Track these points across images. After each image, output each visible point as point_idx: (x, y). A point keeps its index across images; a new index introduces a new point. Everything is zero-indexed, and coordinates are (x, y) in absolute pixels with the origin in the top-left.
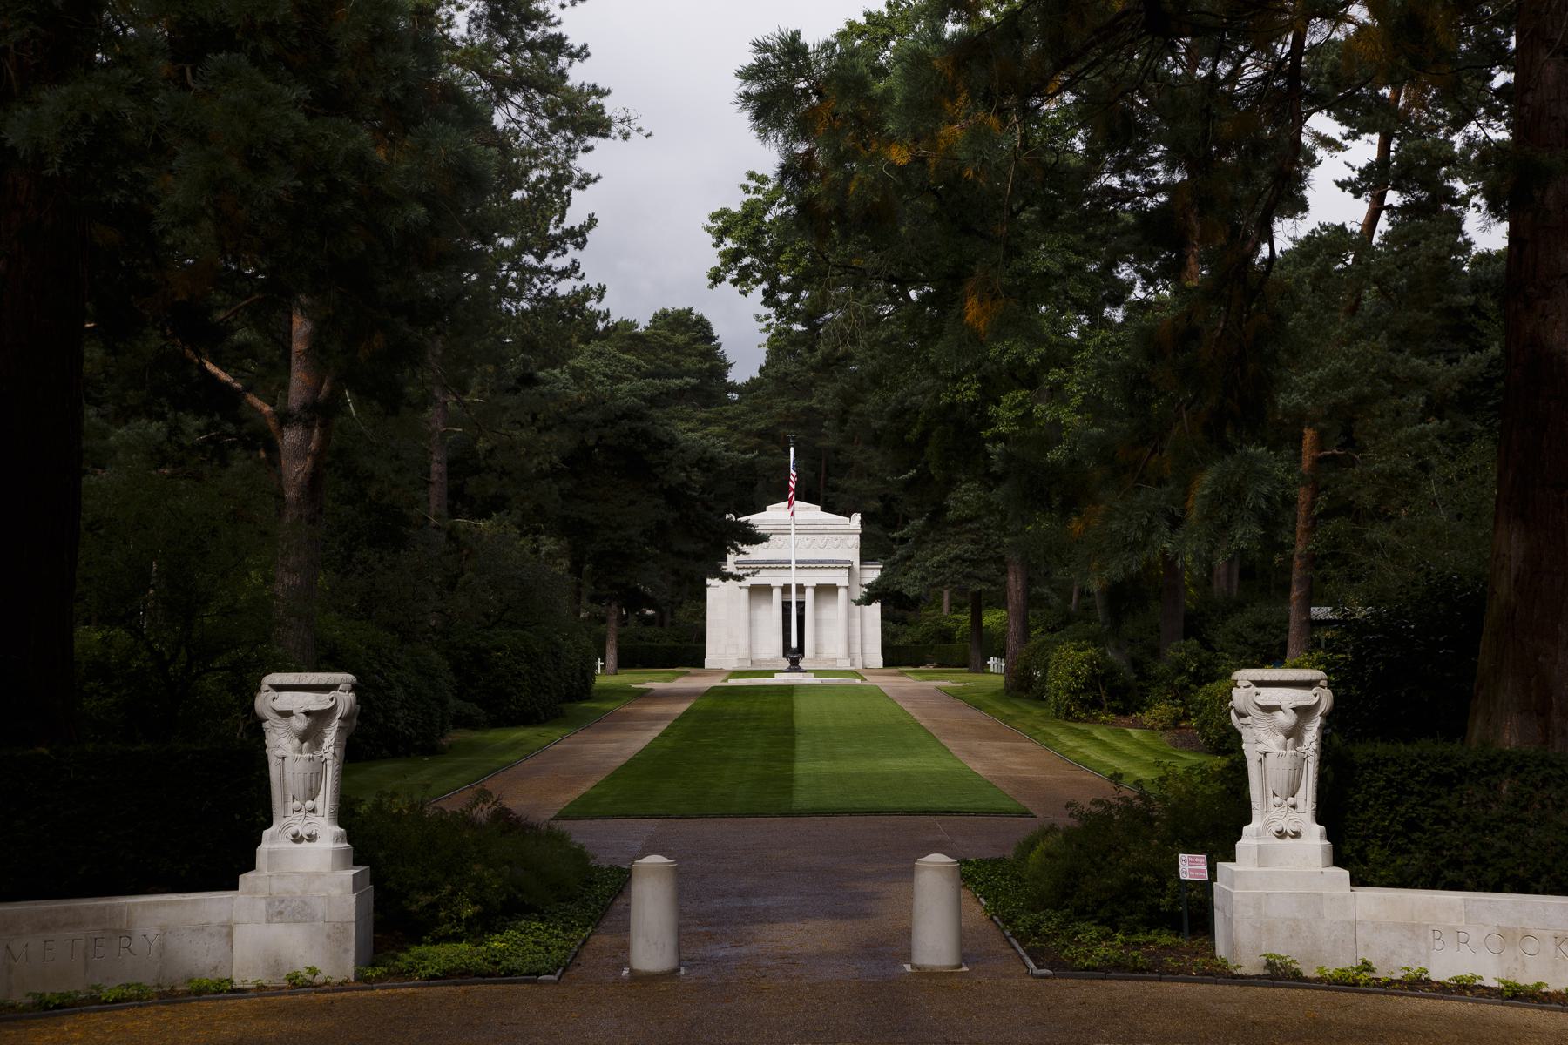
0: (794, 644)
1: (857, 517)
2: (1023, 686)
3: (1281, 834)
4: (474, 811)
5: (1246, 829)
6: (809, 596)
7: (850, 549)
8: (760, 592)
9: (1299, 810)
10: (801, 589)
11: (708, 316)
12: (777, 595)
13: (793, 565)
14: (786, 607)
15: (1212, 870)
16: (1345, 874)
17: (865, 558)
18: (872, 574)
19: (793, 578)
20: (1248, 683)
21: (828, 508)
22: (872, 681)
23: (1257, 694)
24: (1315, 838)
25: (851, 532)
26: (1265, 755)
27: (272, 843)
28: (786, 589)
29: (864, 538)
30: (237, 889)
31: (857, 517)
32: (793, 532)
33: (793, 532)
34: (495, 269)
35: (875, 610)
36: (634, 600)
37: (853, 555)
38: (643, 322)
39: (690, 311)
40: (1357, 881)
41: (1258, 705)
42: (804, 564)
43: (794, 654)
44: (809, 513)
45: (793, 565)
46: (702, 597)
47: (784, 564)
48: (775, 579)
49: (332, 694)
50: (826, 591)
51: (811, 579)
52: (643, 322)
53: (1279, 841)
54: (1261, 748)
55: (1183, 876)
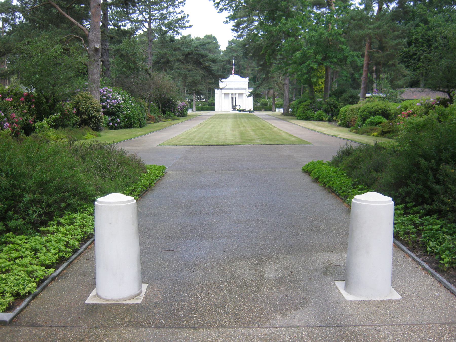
0: (234, 105)
1: (248, 78)
2: (286, 113)
6: (237, 96)
10: (235, 94)
11: (216, 37)
12: (230, 96)
13: (234, 89)
14: (232, 98)
17: (249, 87)
18: (251, 90)
19: (234, 92)
21: (241, 76)
28: (232, 94)
31: (248, 78)
34: (87, 14)
35: (251, 98)
36: (199, 93)
38: (226, 49)
39: (212, 35)
42: (236, 89)
44: (238, 77)
45: (234, 89)
46: (214, 96)
47: (231, 89)
48: (230, 92)
50: (241, 94)
51: (238, 92)
52: (226, 49)
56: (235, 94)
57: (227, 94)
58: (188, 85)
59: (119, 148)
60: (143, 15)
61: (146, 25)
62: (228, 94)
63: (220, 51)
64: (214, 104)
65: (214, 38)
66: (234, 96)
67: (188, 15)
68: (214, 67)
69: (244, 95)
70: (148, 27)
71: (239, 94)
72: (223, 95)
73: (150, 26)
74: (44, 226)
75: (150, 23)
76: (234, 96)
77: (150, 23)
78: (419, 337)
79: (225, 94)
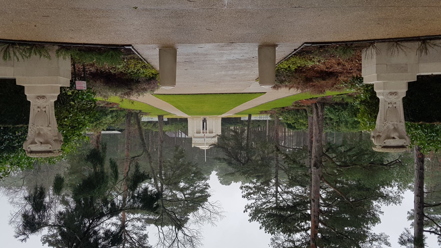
0: (205, 123)
1: (193, 146)
3: (43, 97)
4: (87, 67)
5: (56, 99)
6: (202, 131)
7: (194, 140)
8: (211, 132)
9: (37, 106)
12: (208, 131)
14: (206, 129)
15: (73, 83)
16: (18, 83)
20: (54, 152)
22: (190, 116)
23: (50, 148)
24: (30, 96)
25: (194, 144)
26: (48, 126)
27: (403, 91)
29: (191, 143)
30: (24, 87)
32: (205, 143)
33: (205, 143)
37: (193, 139)
40: (14, 80)
41: (51, 144)
43: (204, 121)
49: (385, 145)
53: (44, 95)
54: (50, 129)
55: (85, 82)
56: (203, 133)
57: (211, 132)
58: (301, 217)
59: (299, 91)
60: (282, 198)
61: (279, 190)
62: (209, 133)
63: (216, 171)
64: (222, 124)
65: (222, 183)
66: (205, 131)
67: (244, 197)
68: (222, 155)
69: (196, 132)
70: (278, 188)
71: (200, 133)
72: (214, 132)
73: (277, 189)
74: (104, 85)
75: (277, 191)
76: (205, 131)
77: (277, 191)
78: (136, 15)
79: (212, 133)
